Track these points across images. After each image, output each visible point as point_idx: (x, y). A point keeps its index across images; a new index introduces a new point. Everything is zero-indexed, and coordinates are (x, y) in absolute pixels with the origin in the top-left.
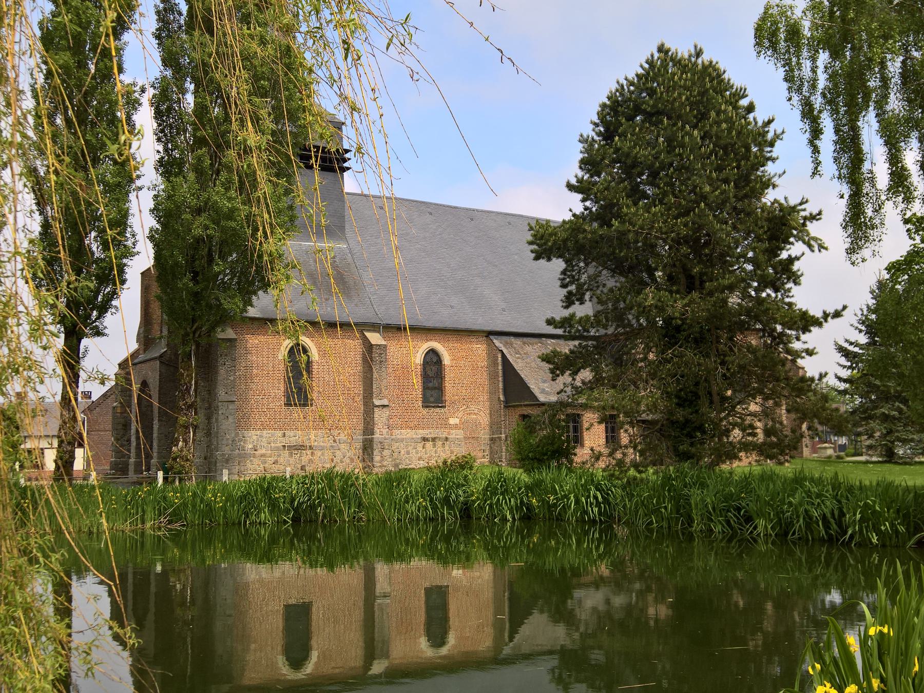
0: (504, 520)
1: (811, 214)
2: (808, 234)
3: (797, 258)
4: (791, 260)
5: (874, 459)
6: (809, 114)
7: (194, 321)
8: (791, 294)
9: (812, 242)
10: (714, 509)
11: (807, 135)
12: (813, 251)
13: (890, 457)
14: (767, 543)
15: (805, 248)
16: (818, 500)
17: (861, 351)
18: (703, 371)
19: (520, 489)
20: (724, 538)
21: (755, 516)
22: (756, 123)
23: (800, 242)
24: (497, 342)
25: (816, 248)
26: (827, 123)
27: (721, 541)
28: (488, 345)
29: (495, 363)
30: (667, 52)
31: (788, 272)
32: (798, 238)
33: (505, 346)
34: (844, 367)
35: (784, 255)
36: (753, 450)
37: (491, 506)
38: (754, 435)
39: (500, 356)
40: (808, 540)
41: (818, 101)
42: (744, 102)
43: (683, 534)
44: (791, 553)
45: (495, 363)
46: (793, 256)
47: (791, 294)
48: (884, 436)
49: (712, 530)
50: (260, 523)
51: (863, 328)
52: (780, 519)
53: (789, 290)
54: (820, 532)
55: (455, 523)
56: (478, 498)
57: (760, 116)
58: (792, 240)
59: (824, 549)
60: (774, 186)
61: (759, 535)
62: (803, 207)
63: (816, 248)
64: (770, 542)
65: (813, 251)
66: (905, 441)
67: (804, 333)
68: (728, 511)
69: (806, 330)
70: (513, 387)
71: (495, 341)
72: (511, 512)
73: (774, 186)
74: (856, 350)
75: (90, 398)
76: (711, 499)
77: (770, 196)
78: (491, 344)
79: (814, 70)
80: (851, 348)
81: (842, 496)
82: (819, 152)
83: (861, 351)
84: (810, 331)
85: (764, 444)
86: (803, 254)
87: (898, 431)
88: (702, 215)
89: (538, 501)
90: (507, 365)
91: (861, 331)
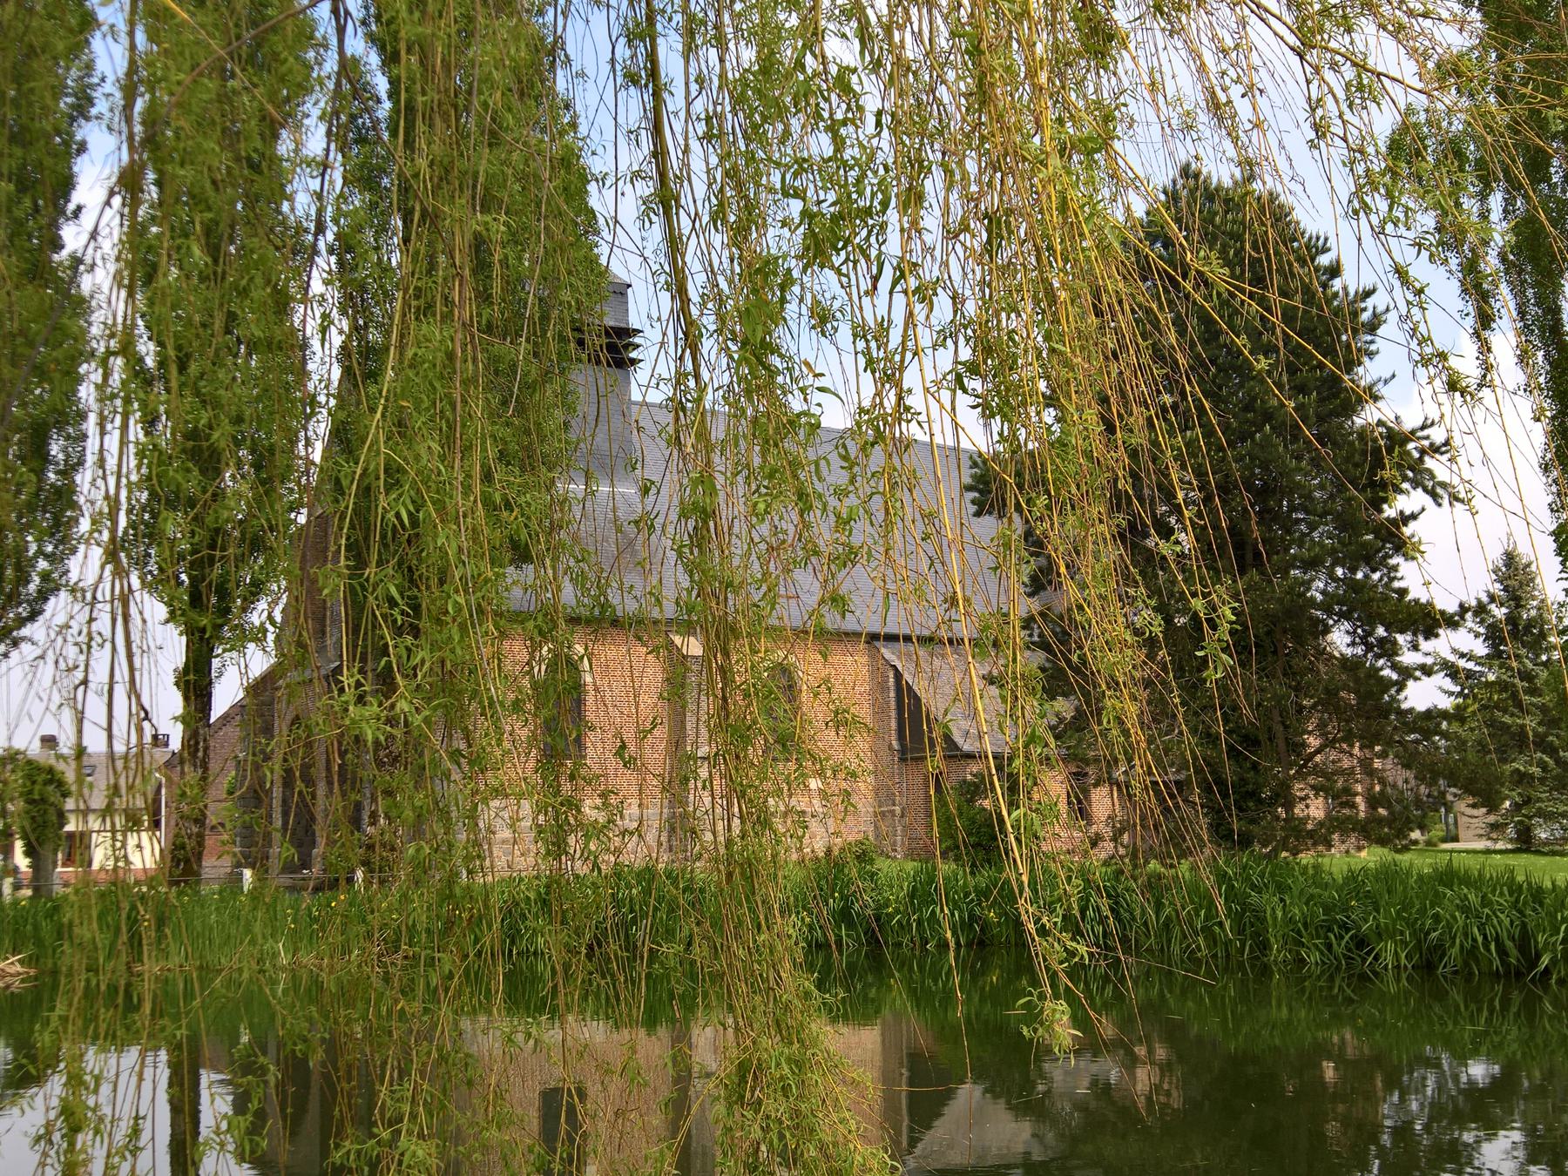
0: (943, 946)
1: (1432, 445)
2: (1433, 477)
3: (1414, 517)
4: (1406, 519)
5: (1500, 846)
6: (1476, 288)
7: (995, 644)
8: (1399, 575)
9: (1439, 490)
10: (1305, 925)
11: (1470, 322)
12: (1440, 505)
13: (1525, 842)
14: (1398, 980)
15: (1427, 500)
16: (1486, 910)
17: (1478, 668)
18: (1268, 700)
19: (967, 895)
20: (1323, 972)
21: (1373, 937)
22: (1347, 294)
23: (1420, 490)
24: (887, 652)
25: (1445, 502)
26: (1505, 299)
27: (1319, 978)
28: (872, 657)
29: (883, 688)
30: (1197, 176)
31: (1394, 538)
32: (1416, 484)
33: (899, 658)
34: (1451, 694)
35: (1389, 512)
36: (1353, 830)
37: (919, 922)
38: (1354, 806)
39: (891, 674)
40: (1471, 974)
41: (1491, 263)
42: (1324, 260)
43: (1253, 967)
44: (1440, 996)
45: (883, 688)
46: (1407, 513)
47: (1399, 575)
48: (1517, 807)
49: (1303, 961)
50: (535, 953)
51: (1482, 630)
52: (1419, 941)
53: (1395, 568)
54: (1491, 962)
55: (858, 951)
56: (897, 911)
57: (1350, 281)
58: (1405, 486)
59: (1499, 988)
60: (1376, 398)
61: (1386, 967)
62: (1425, 433)
63: (1445, 502)
64: (1404, 976)
65: (1440, 505)
66: (1549, 817)
67: (1426, 639)
68: (1330, 930)
69: (1430, 634)
70: (912, 727)
71: (883, 650)
72: (954, 933)
73: (1376, 398)
74: (1470, 665)
75: (167, 745)
76: (1301, 910)
77: (1368, 415)
78: (874, 655)
79: (1484, 216)
80: (1462, 663)
81: (1525, 903)
82: (1489, 350)
83: (1478, 668)
84: (1437, 636)
85: (1368, 820)
86: (1423, 509)
87: (1539, 800)
88: (1266, 444)
89: (999, 916)
90: (905, 693)
91: (1477, 635)
